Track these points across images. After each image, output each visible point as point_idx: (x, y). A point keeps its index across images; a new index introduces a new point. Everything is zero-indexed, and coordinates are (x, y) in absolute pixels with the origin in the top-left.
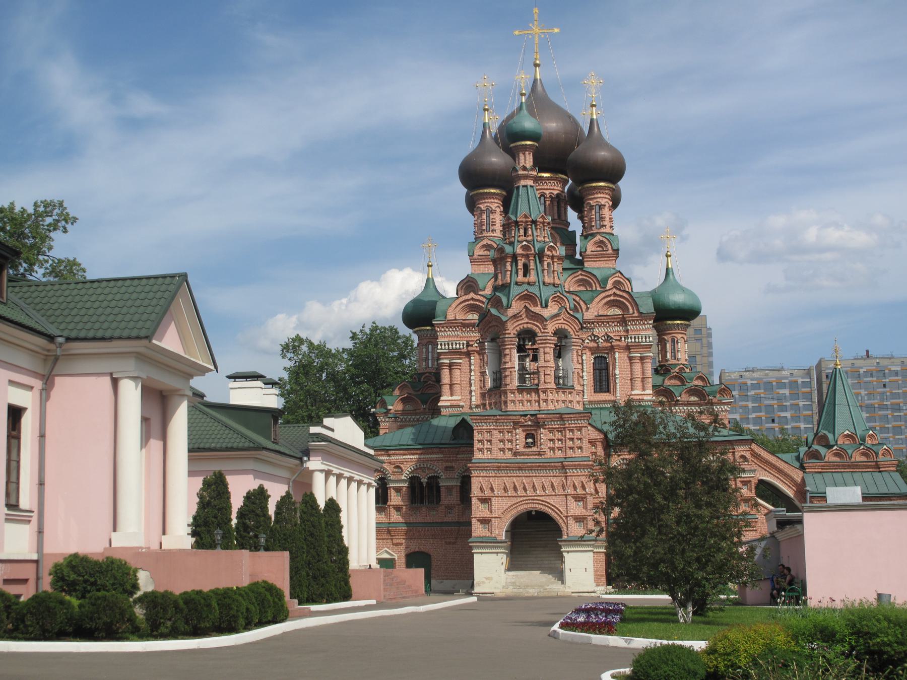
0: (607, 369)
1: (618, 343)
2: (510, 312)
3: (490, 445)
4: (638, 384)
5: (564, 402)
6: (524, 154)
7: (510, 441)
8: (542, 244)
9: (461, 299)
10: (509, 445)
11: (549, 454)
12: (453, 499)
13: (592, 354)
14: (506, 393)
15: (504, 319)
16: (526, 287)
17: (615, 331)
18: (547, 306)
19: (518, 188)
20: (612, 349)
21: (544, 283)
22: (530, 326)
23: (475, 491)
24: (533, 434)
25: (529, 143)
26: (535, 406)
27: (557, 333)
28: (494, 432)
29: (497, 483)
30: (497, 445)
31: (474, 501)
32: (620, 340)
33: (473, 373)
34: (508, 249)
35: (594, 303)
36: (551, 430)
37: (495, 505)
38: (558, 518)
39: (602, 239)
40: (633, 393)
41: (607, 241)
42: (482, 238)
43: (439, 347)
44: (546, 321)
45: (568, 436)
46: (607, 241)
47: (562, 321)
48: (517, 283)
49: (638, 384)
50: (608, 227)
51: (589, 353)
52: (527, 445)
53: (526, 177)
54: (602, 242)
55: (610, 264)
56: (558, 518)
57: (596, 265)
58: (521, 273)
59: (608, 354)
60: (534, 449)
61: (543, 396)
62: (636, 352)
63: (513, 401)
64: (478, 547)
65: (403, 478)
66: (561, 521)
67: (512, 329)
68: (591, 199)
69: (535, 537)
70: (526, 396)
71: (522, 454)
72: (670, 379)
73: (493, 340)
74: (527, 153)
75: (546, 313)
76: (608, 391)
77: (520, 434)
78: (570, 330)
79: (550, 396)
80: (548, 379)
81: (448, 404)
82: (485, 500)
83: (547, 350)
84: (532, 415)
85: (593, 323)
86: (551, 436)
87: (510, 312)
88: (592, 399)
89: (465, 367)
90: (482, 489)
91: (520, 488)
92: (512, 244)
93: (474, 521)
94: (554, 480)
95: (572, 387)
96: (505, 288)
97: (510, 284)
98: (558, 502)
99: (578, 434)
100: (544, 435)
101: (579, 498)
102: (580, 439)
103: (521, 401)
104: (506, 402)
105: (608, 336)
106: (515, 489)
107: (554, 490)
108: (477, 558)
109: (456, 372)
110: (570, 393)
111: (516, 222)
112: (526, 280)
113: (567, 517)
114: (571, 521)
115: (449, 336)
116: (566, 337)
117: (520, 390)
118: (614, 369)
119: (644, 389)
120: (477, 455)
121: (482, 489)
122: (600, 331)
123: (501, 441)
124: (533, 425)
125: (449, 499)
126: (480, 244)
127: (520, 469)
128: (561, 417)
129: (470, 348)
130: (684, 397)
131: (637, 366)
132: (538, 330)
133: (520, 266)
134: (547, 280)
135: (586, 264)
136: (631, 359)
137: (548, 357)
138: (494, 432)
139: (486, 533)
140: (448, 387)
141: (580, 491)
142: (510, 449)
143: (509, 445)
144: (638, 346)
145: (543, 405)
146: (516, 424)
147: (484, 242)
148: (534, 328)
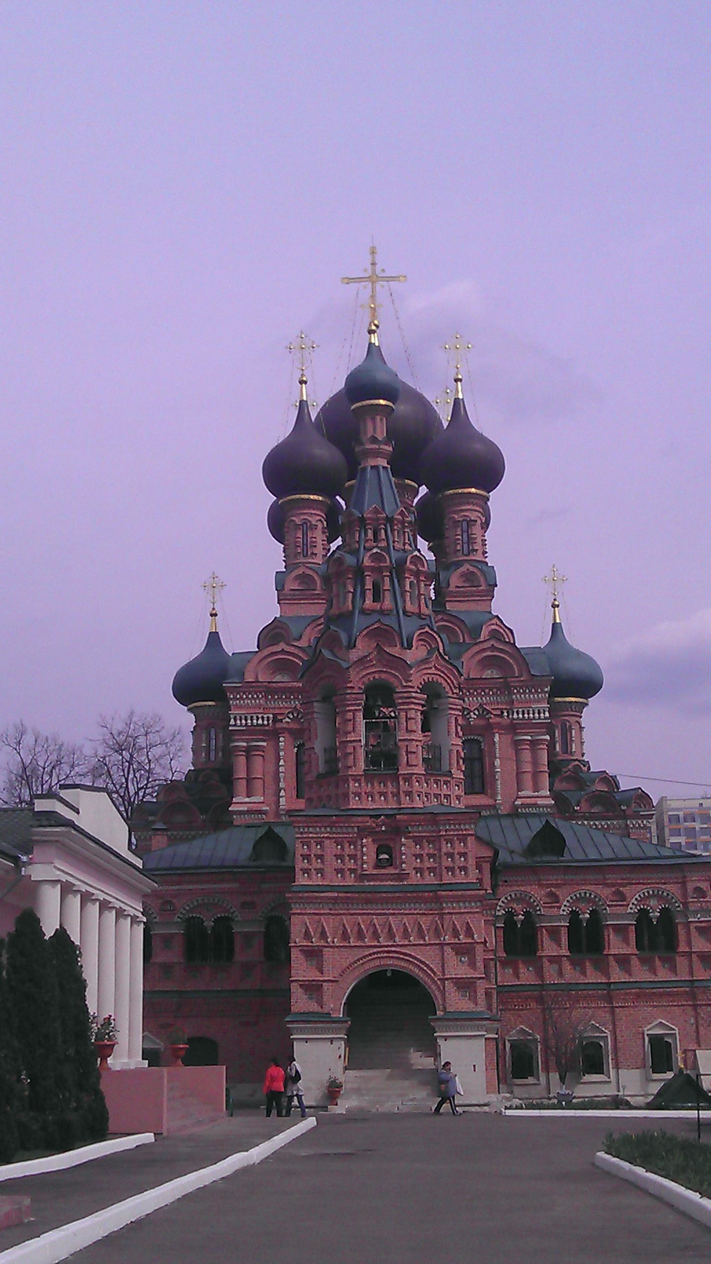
0: (481, 759)
1: (498, 720)
2: (354, 655)
3: (322, 864)
4: (528, 779)
5: (437, 796)
8: (401, 554)
9: (266, 652)
10: (351, 864)
11: (415, 879)
12: (248, 954)
14: (347, 781)
15: (345, 665)
16: (376, 617)
17: (490, 701)
18: (410, 647)
19: (365, 469)
20: (488, 729)
21: (405, 612)
22: (383, 676)
23: (297, 938)
24: (388, 847)
25: (382, 402)
28: (327, 842)
30: (332, 863)
33: (282, 763)
34: (350, 560)
36: (418, 841)
37: (329, 960)
39: (472, 569)
42: (297, 566)
43: (232, 722)
44: (410, 667)
47: (433, 671)
48: (363, 612)
49: (528, 779)
50: (480, 552)
52: (379, 864)
53: (377, 454)
55: (480, 607)
57: (463, 607)
58: (369, 596)
61: (404, 786)
62: (526, 734)
64: (301, 1030)
65: (176, 919)
66: (434, 987)
67: (357, 680)
68: (455, 512)
69: (391, 1011)
70: (378, 788)
72: (561, 780)
73: (326, 699)
74: (378, 418)
75: (410, 656)
76: (482, 791)
77: (369, 847)
78: (445, 684)
80: (413, 760)
81: (244, 808)
82: (313, 954)
83: (412, 714)
87: (354, 655)
89: (270, 755)
90: (307, 936)
92: (355, 552)
93: (294, 987)
94: (422, 920)
95: (449, 774)
96: (345, 618)
97: (352, 613)
98: (429, 956)
99: (460, 847)
100: (407, 848)
101: (461, 950)
102: (464, 855)
104: (346, 796)
106: (360, 935)
108: (299, 1049)
109: (258, 762)
111: (362, 520)
112: (378, 606)
113: (443, 980)
115: (247, 707)
116: (438, 696)
117: (368, 777)
119: (536, 790)
120: (301, 880)
121: (307, 936)
123: (337, 857)
124: (389, 832)
125: (248, 954)
126: (294, 574)
127: (368, 901)
128: (432, 818)
129: (279, 725)
130: (583, 807)
132: (395, 682)
133: (369, 586)
134: (409, 607)
135: (448, 606)
136: (517, 744)
137: (412, 726)
139: (315, 1007)
140: (244, 781)
143: (351, 864)
144: (529, 725)
145: (406, 802)
146: (363, 832)
147: (300, 571)
148: (393, 680)
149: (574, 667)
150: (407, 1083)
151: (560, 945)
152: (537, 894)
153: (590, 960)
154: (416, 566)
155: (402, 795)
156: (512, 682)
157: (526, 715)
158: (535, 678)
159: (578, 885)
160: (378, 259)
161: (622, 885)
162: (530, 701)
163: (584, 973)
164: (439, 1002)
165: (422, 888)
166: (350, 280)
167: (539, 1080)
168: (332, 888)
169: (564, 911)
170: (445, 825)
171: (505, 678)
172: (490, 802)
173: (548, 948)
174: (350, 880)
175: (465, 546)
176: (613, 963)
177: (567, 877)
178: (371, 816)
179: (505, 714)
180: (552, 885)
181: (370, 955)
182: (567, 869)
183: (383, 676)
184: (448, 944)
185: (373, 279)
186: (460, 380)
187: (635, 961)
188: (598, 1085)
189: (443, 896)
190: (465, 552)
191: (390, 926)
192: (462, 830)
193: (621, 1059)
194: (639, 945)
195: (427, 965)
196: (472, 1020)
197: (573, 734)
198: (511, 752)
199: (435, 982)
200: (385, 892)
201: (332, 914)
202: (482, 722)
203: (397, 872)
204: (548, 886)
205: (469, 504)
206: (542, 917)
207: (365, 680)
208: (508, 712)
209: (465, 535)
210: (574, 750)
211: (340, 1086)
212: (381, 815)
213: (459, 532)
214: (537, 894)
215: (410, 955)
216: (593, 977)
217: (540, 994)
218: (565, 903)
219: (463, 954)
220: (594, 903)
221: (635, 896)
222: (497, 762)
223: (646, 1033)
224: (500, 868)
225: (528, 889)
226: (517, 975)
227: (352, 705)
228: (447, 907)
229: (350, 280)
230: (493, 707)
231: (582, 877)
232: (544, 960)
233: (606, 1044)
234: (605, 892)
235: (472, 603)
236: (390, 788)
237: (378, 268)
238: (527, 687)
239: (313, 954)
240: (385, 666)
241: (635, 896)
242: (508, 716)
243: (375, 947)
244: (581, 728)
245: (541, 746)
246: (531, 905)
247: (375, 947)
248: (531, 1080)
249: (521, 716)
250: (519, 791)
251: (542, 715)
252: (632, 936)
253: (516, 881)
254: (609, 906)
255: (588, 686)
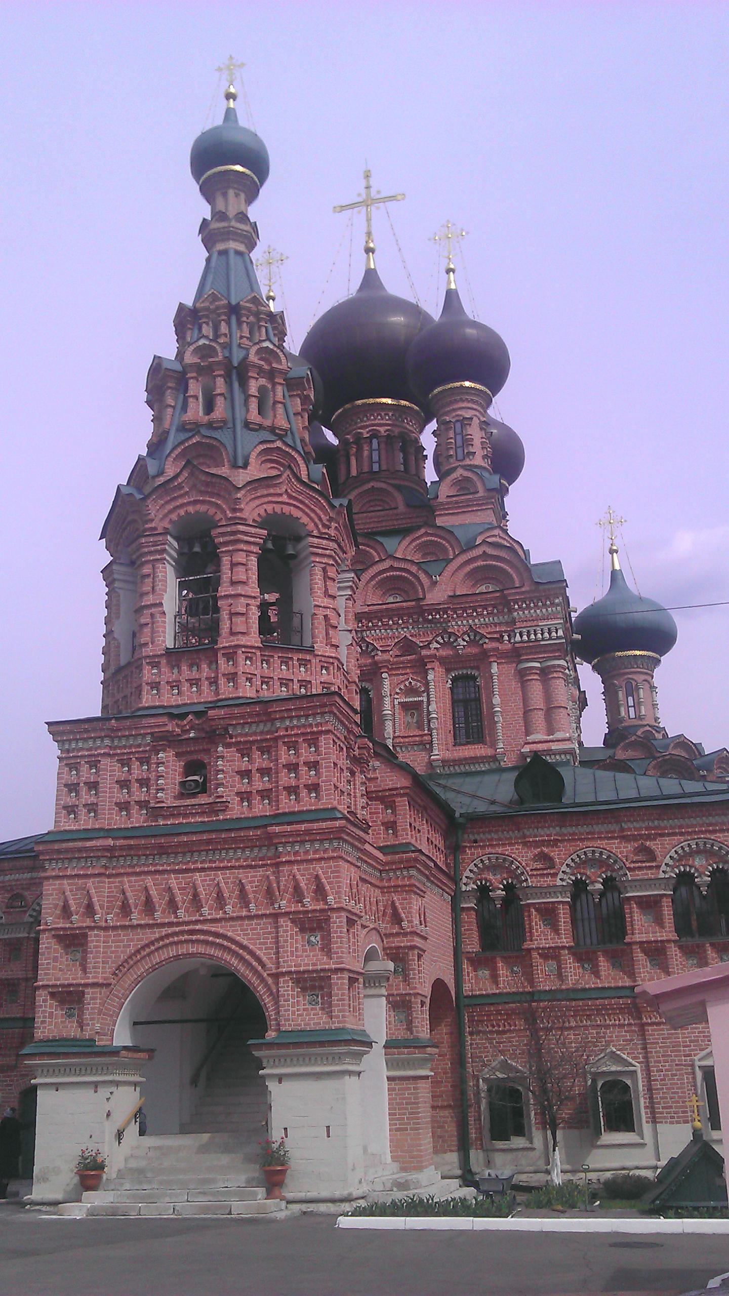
0: (478, 700)
1: (495, 645)
4: (539, 719)
6: (225, 195)
7: (144, 783)
10: (139, 794)
11: (237, 810)
13: (448, 671)
20: (484, 658)
22: (202, 508)
23: (51, 918)
26: (207, 694)
27: (267, 522)
28: (105, 762)
29: (102, 892)
31: (47, 943)
32: (500, 640)
35: (445, 574)
36: (244, 750)
38: (255, 981)
39: (469, 474)
40: (530, 738)
41: (475, 478)
45: (283, 760)
46: (475, 478)
47: (285, 498)
49: (539, 719)
51: (440, 670)
52: (186, 790)
54: (467, 479)
56: (255, 981)
59: (477, 668)
60: (203, 799)
61: (223, 665)
63: (155, 685)
66: (261, 989)
68: (447, 414)
70: (186, 672)
71: (172, 812)
72: (625, 749)
74: (231, 193)
79: (244, 665)
82: (74, 941)
83: (240, 558)
84: (198, 714)
85: (445, 611)
86: (244, 764)
88: (448, 755)
90: (66, 911)
91: (160, 902)
95: (311, 650)
98: (252, 936)
99: (306, 753)
100: (227, 763)
103: (175, 685)
105: (476, 633)
106: (149, 906)
107: (246, 904)
110: (304, 663)
113: (276, 976)
114: (287, 987)
118: (491, 694)
121: (66, 911)
122: (457, 626)
127: (163, 851)
131: (536, 689)
136: (522, 676)
138: (105, 762)
139: (72, 1030)
141: (310, 903)
142: (142, 804)
143: (139, 794)
144: (536, 649)
145: (226, 690)
149: (640, 616)
150: (224, 1159)
151: (556, 931)
152: (522, 857)
153: (606, 953)
154: (270, 364)
155: (222, 681)
156: (510, 594)
157: (533, 636)
158: (541, 587)
159: (582, 840)
160: (372, 182)
161: (649, 837)
162: (538, 619)
163: (597, 974)
164: (271, 1012)
165: (246, 824)
166: (343, 208)
167: (531, 1143)
168: (108, 833)
169: (564, 878)
170: (282, 719)
171: (502, 591)
172: (490, 752)
173: (540, 936)
174: (138, 818)
175: (460, 451)
176: (640, 956)
177: (564, 830)
178: (172, 716)
179: (506, 638)
180: (542, 843)
181: (162, 938)
182: (564, 818)
183: (202, 508)
184: (287, 914)
185: (368, 202)
186: (453, 271)
187: (674, 952)
188: (625, 1150)
189: (277, 835)
190: (460, 456)
191: (195, 888)
192: (311, 725)
193: (659, 1108)
194: (683, 927)
195: (252, 953)
196: (322, 1044)
197: (642, 696)
198: (515, 685)
199: (263, 980)
200: (185, 834)
201: (109, 876)
202: (474, 650)
203: (211, 800)
204: (537, 844)
205: (462, 400)
206: (528, 891)
207: (174, 517)
208: (509, 636)
209: (459, 438)
210: (643, 713)
211: (101, 1167)
212: (187, 714)
213: (451, 434)
214: (522, 857)
215: (225, 937)
216: (609, 976)
217: (528, 1008)
218: (564, 868)
219: (312, 930)
220: (610, 867)
221: (668, 851)
222: (496, 700)
223: (697, 1063)
224: (461, 820)
225: (508, 850)
226: (495, 978)
227: (150, 553)
228: (286, 852)
229: (343, 208)
230: (489, 630)
231: (586, 829)
232: (535, 954)
233: (635, 1082)
234: (622, 850)
235: (468, 515)
236: (206, 671)
237: (373, 192)
238: (531, 601)
239: (74, 941)
240: (202, 493)
241: (668, 851)
242: (509, 641)
243: (170, 924)
244: (653, 688)
245: (555, 675)
246: (512, 873)
247: (170, 924)
248: (518, 1142)
249: (525, 638)
250: (527, 735)
251: (554, 634)
252: (667, 912)
253: (492, 840)
254: (629, 869)
255: (659, 639)
